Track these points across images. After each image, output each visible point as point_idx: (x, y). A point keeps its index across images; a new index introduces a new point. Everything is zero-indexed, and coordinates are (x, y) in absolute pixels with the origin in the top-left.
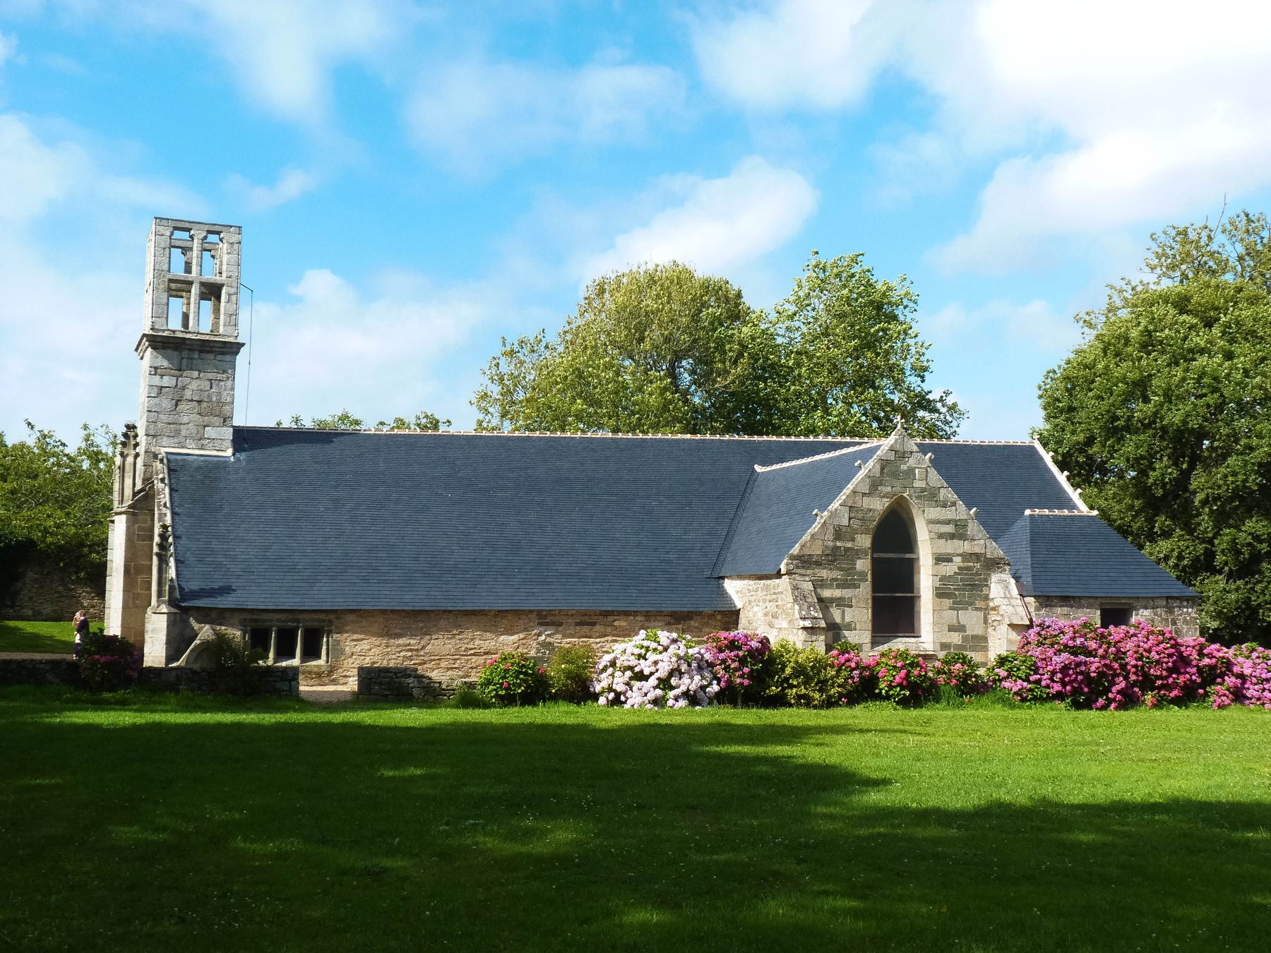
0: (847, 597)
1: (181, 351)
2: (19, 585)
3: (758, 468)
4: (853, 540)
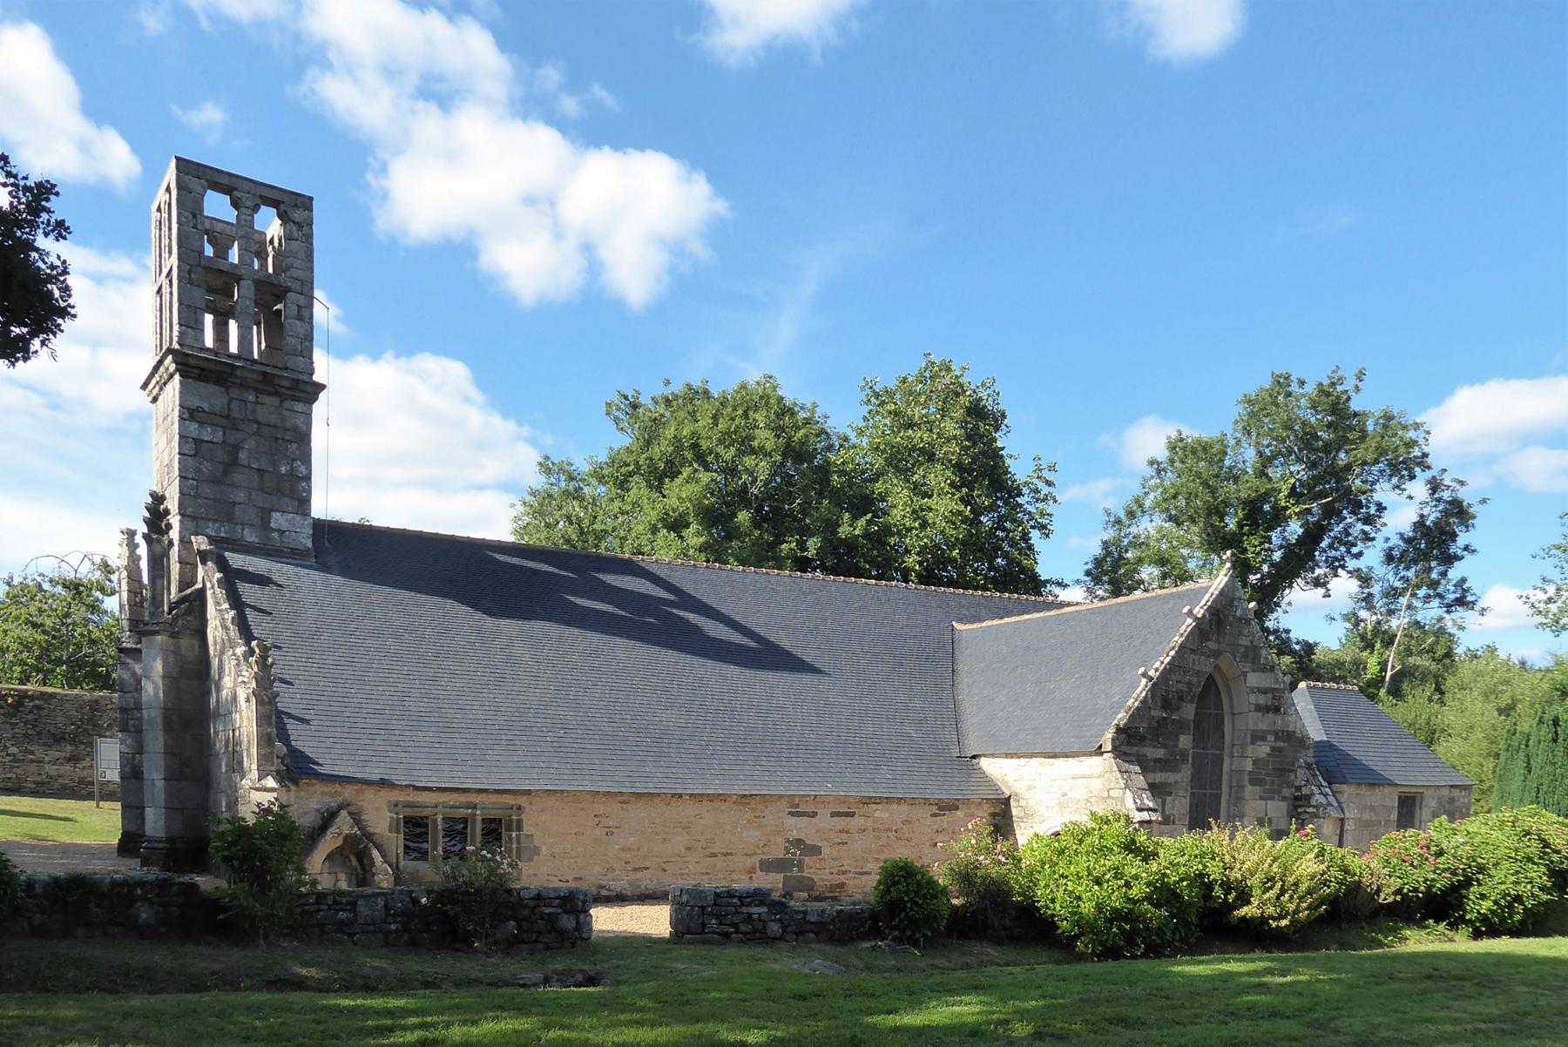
1: (227, 388)
2: (941, 874)
3: (958, 626)
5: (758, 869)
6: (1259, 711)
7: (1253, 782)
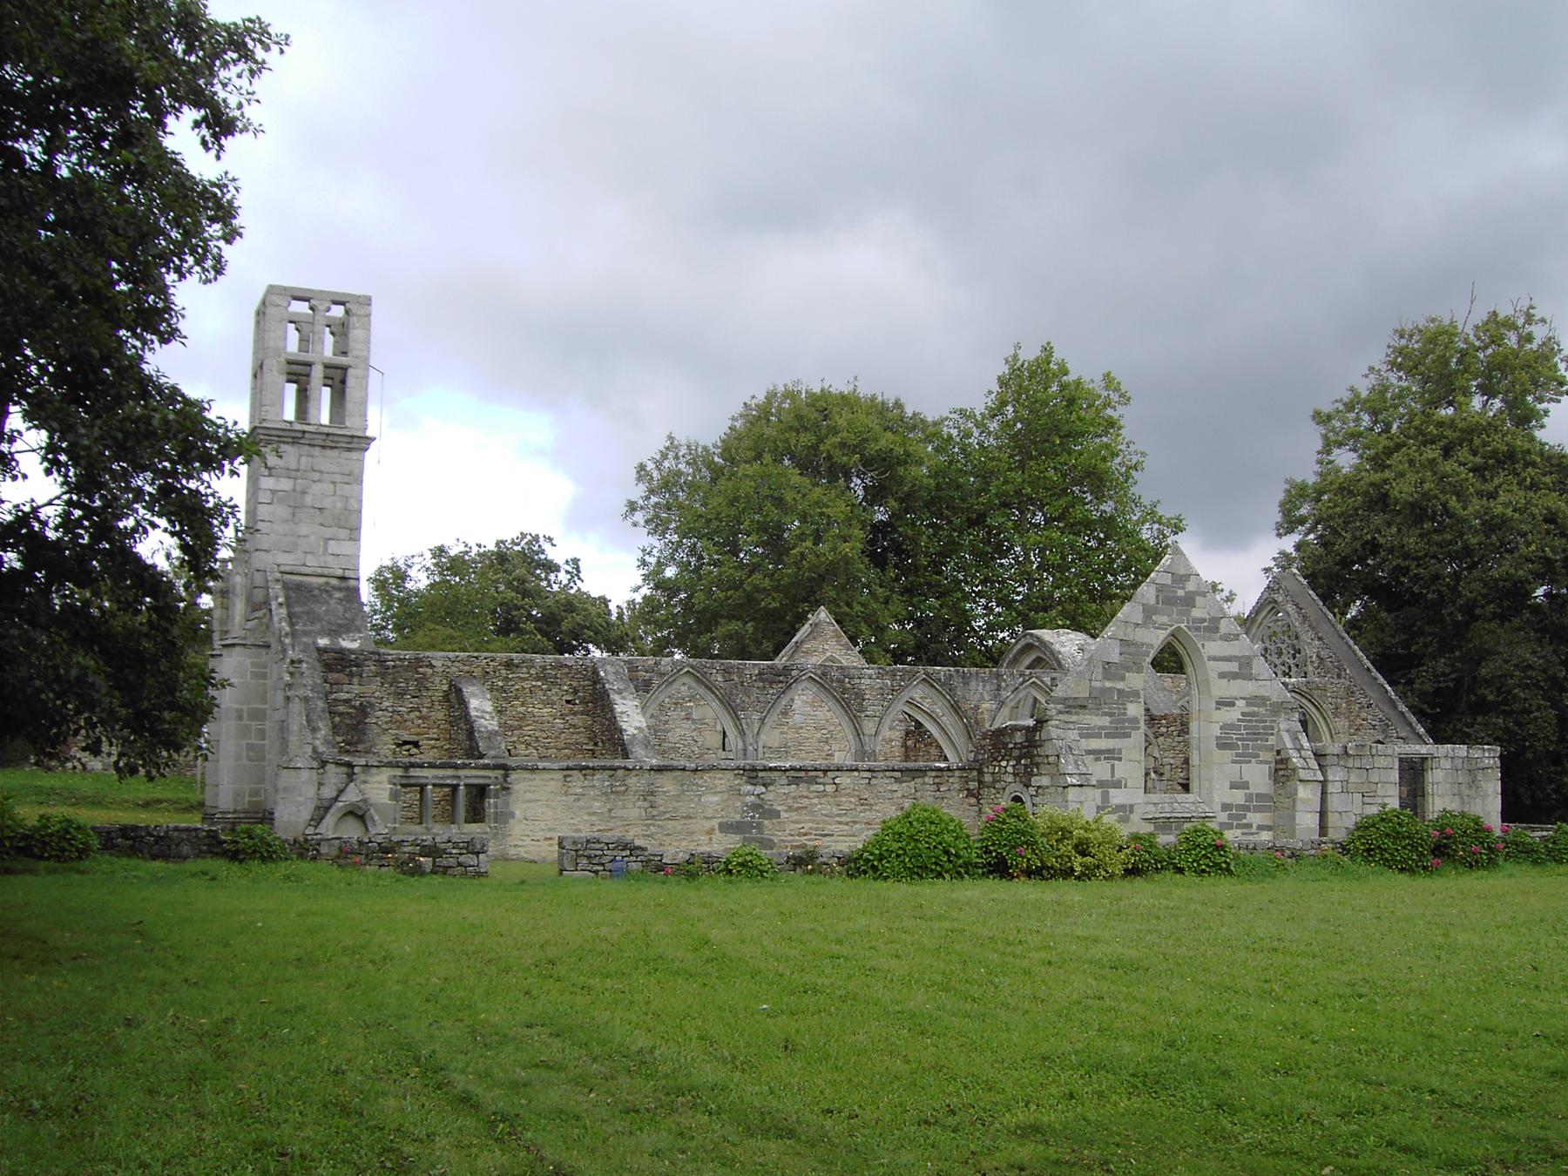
0: (266, 763)
4: (1123, 679)
5: (717, 831)
6: (1223, 677)
7: (1223, 745)
